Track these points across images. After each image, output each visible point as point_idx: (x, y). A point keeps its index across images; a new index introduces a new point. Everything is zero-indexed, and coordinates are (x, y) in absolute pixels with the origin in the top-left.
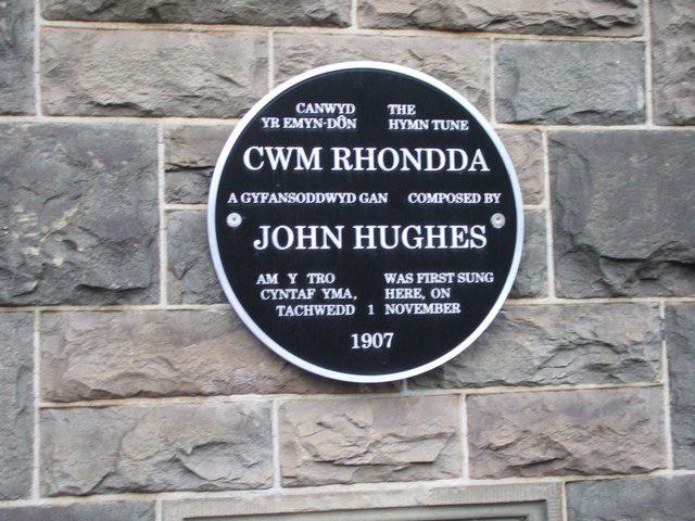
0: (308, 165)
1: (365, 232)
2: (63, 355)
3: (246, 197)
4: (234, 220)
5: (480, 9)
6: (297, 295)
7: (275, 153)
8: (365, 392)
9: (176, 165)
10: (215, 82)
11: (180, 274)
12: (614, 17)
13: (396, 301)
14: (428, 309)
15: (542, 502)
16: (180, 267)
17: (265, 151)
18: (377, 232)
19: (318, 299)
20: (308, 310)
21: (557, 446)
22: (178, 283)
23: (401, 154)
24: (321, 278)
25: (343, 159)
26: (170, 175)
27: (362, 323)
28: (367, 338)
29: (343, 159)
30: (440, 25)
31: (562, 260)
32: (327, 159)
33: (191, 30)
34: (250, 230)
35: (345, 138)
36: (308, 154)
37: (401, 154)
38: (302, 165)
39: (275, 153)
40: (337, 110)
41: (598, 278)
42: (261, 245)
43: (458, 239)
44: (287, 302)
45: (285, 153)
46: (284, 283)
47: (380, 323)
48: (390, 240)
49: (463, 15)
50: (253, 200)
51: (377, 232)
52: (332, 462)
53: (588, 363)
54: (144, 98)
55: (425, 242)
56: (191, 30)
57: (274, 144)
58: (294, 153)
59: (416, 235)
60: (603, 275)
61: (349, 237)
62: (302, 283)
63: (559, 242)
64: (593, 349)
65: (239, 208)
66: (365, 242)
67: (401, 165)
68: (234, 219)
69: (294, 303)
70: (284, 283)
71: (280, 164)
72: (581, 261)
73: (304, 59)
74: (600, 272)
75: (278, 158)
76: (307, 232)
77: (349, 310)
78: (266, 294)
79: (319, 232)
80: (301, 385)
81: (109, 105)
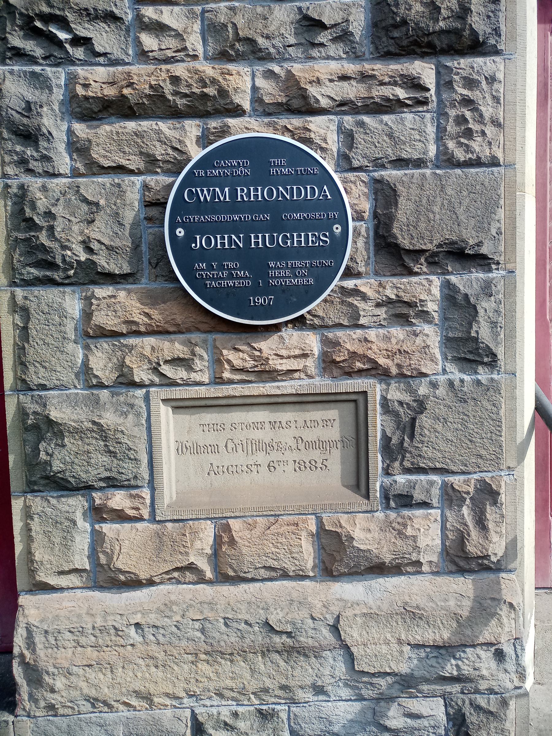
0: (222, 199)
1: (257, 237)
2: (91, 311)
3: (186, 218)
4: (180, 232)
5: (329, 97)
6: (217, 275)
7: (202, 191)
8: (262, 331)
9: (148, 202)
10: (170, 151)
11: (154, 265)
12: (415, 98)
13: (276, 277)
14: (295, 281)
15: (366, 392)
16: (154, 261)
17: (196, 191)
18: (264, 238)
19: (231, 277)
20: (224, 283)
21: (373, 361)
22: (153, 270)
23: (278, 190)
24: (231, 265)
25: (243, 194)
26: (147, 208)
27: (256, 291)
28: (258, 299)
29: (243, 194)
30: (303, 109)
31: (379, 252)
32: (234, 193)
33: (187, 726)
34: (190, 238)
35: (247, 182)
36: (222, 191)
37: (278, 190)
38: (219, 198)
39: (202, 191)
40: (239, 163)
41: (401, 262)
42: (196, 246)
43: (312, 241)
44: (213, 279)
45: (209, 191)
46: (210, 268)
47: (267, 290)
48: (272, 241)
49: (317, 101)
50: (190, 220)
51: (264, 238)
52: (242, 369)
53: (394, 313)
54: (128, 162)
55: (293, 243)
56: (187, 726)
57: (201, 186)
58: (214, 190)
59: (288, 239)
60: (404, 261)
61: (247, 240)
62: (221, 267)
63: (513, 265)
64: (397, 305)
65: (183, 225)
66: (257, 243)
67: (278, 196)
68: (180, 232)
69: (215, 280)
70: (210, 268)
71: (205, 198)
72: (390, 253)
73: (221, 135)
74: (401, 259)
75: (204, 194)
76: (223, 238)
77: (248, 283)
78: (199, 274)
79: (230, 238)
80: (225, 328)
81: (109, 167)
